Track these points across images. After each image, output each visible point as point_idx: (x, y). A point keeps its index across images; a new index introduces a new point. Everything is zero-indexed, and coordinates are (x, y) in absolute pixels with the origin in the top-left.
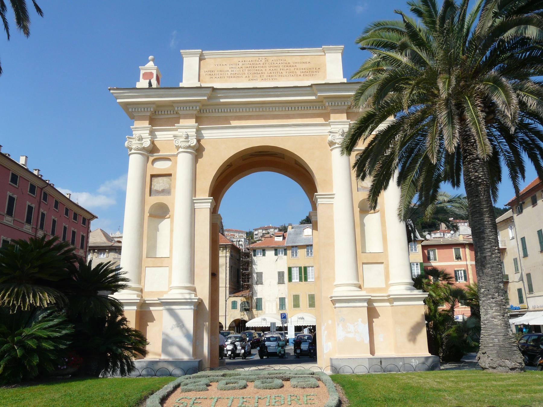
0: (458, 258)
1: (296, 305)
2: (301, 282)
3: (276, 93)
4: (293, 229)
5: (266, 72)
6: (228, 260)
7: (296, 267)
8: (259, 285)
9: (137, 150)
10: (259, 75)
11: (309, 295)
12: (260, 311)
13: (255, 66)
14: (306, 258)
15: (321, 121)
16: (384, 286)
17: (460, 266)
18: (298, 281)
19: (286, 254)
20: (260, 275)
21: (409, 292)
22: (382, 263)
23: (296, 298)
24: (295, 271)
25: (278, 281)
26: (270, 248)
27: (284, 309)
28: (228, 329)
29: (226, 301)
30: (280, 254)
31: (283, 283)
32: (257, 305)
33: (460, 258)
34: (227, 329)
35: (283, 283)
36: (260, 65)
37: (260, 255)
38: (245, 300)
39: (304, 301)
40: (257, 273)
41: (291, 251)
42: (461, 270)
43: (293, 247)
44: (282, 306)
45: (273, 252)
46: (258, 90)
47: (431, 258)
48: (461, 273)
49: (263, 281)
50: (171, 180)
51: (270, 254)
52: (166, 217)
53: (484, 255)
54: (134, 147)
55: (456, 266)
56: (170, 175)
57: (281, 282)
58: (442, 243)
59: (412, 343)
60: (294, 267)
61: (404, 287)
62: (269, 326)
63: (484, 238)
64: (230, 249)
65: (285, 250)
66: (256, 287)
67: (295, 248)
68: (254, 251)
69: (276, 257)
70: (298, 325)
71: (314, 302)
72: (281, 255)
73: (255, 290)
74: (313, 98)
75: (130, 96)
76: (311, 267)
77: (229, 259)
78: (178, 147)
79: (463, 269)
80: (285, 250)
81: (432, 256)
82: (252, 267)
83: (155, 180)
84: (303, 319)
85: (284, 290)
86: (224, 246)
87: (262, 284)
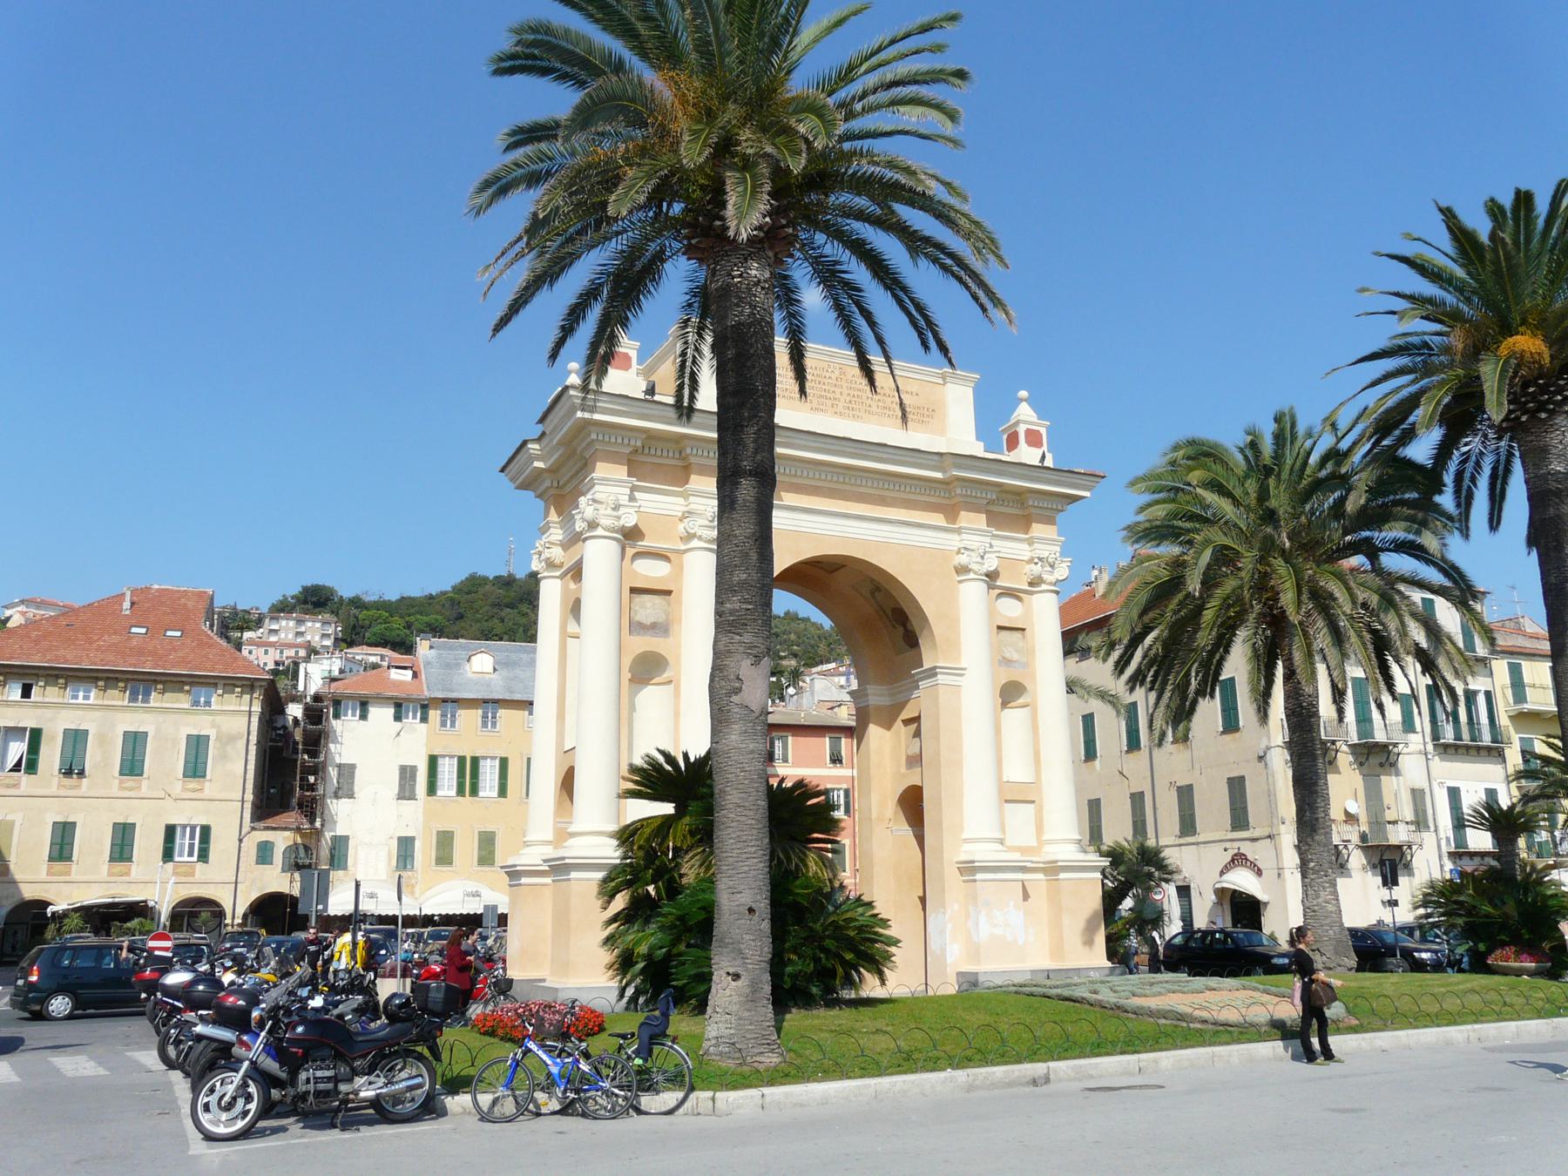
0: (836, 759)
1: (444, 857)
2: (460, 798)
3: (881, 455)
4: (433, 651)
5: (842, 399)
6: (256, 724)
7: (451, 757)
8: (343, 800)
9: (612, 532)
10: (829, 402)
11: (438, 832)
12: (341, 873)
13: (823, 380)
14: (479, 733)
15: (938, 519)
16: (1035, 844)
17: (839, 779)
18: (495, 794)
19: (424, 719)
20: (348, 771)
21: (1082, 856)
22: (1033, 802)
23: (445, 841)
24: (447, 766)
25: (397, 792)
26: (382, 700)
27: (409, 867)
28: (240, 921)
29: (240, 841)
30: (408, 718)
31: (412, 797)
32: (332, 856)
33: (841, 762)
34: (238, 921)
35: (412, 797)
36: (830, 381)
37: (354, 715)
38: (299, 840)
39: (466, 849)
40: (339, 766)
41: (439, 712)
42: (839, 790)
43: (445, 701)
44: (405, 860)
45: (391, 711)
46: (850, 444)
47: (776, 757)
48: (838, 796)
49: (356, 789)
50: (669, 604)
51: (381, 715)
52: (652, 682)
53: (1316, 816)
54: (604, 521)
55: (830, 778)
56: (668, 593)
57: (407, 794)
58: (803, 722)
59: (1087, 948)
60: (444, 756)
61: (1073, 847)
62: (479, 913)
63: (1316, 792)
64: (262, 692)
65: (424, 707)
66: (335, 805)
67: (450, 705)
68: (337, 703)
69: (398, 725)
70: (465, 913)
71: (492, 853)
72: (412, 721)
73: (330, 810)
74: (939, 475)
75: (607, 408)
76: (489, 760)
77: (257, 720)
78: (690, 537)
79: (845, 786)
80: (425, 707)
81: (778, 752)
82: (326, 745)
83: (639, 599)
84: (478, 896)
85: (413, 817)
86: (245, 683)
87: (351, 796)
